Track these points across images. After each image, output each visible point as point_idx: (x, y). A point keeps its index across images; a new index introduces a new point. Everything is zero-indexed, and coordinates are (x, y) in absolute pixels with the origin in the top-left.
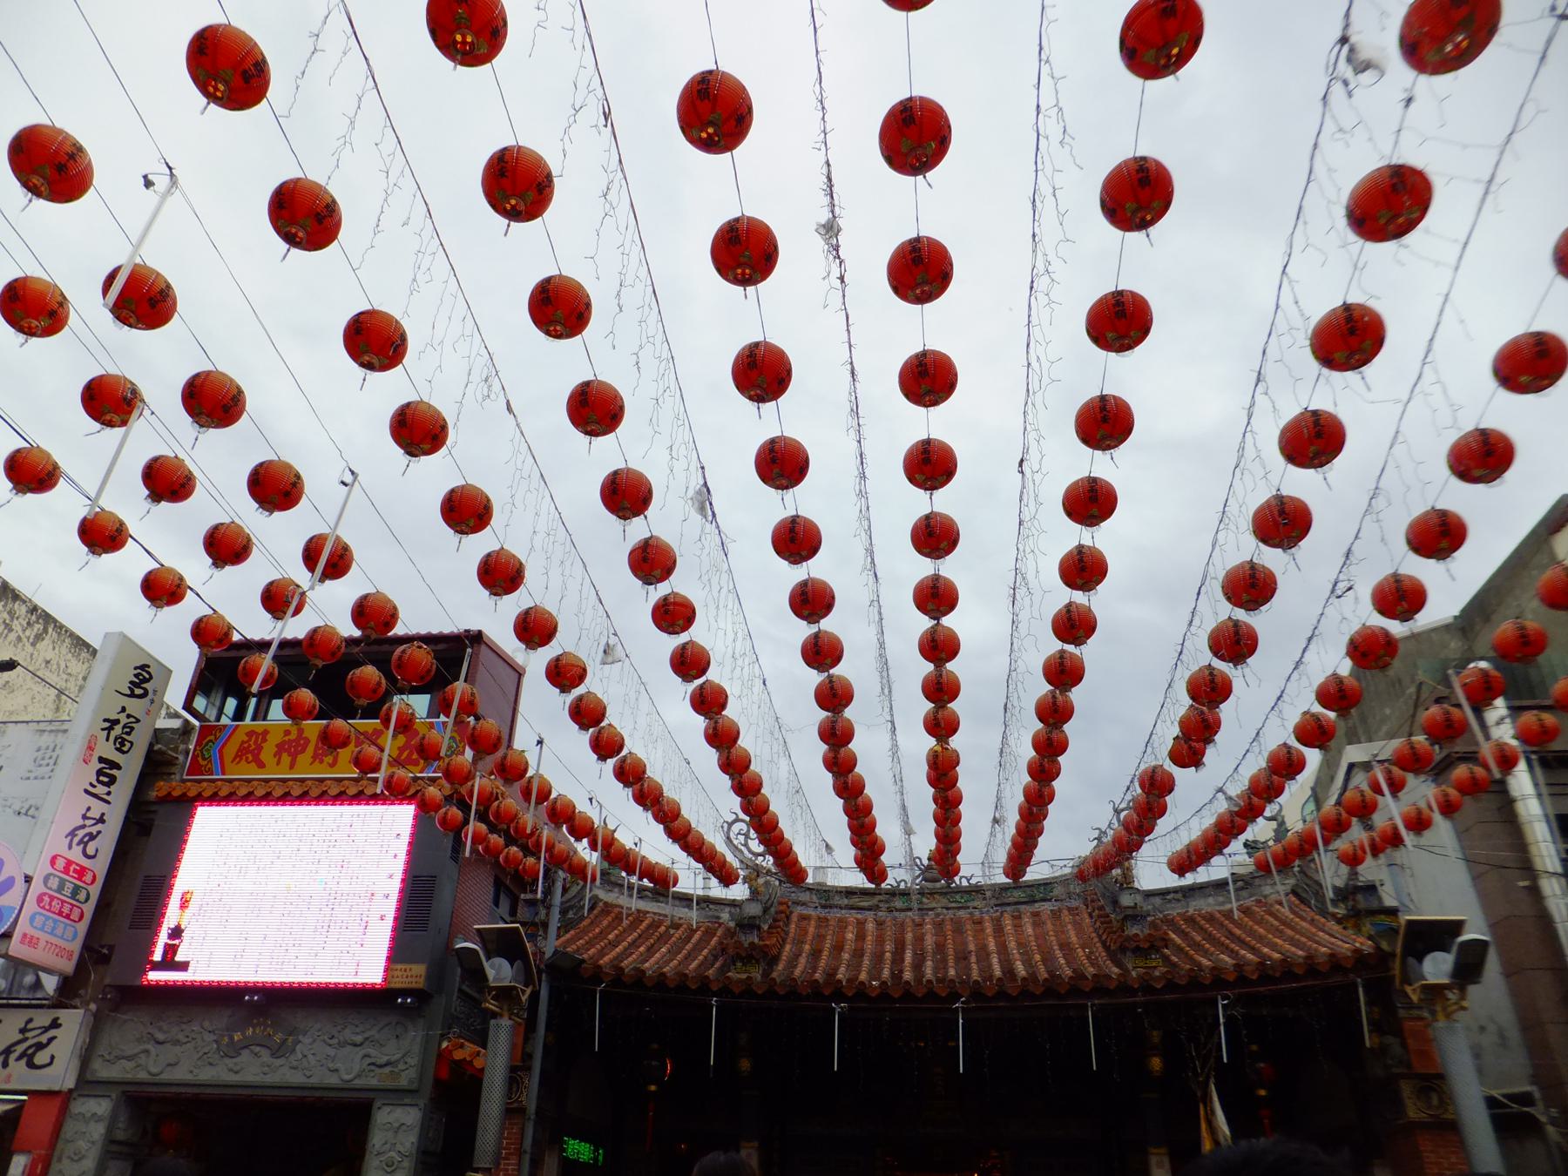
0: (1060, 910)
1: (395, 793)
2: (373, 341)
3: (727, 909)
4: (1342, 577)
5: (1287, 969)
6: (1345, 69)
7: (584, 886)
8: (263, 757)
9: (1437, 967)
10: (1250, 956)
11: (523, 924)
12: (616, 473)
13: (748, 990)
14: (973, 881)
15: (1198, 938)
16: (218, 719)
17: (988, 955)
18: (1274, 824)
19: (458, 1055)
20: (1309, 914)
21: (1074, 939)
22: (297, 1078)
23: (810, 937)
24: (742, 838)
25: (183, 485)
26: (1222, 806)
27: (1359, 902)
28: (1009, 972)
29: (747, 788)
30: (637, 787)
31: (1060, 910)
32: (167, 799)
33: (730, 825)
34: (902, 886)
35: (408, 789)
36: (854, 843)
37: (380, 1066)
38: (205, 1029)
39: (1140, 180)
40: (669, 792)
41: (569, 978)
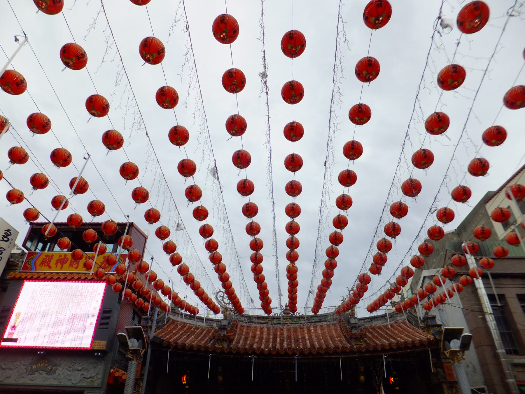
0: (330, 325)
1: (97, 278)
2: (97, 106)
3: (216, 323)
4: (433, 206)
5: (406, 345)
6: (439, 27)
7: (165, 314)
8: (51, 264)
9: (455, 345)
10: (394, 341)
11: (143, 327)
12: (183, 160)
13: (222, 351)
14: (300, 314)
15: (376, 335)
16: (35, 250)
17: (305, 340)
18: (400, 296)
19: (117, 374)
20: (412, 327)
21: (334, 334)
22: (55, 383)
23: (244, 333)
24: (221, 298)
25: (24, 158)
26: (388, 287)
27: (429, 323)
28: (313, 345)
29: (224, 279)
30: (185, 276)
31: (330, 325)
32: (14, 279)
33: (218, 293)
34: (276, 316)
35: (102, 277)
36: (261, 299)
37: (87, 378)
38: (22, 365)
39: (368, 64)
40: (197, 279)
41: (159, 347)
